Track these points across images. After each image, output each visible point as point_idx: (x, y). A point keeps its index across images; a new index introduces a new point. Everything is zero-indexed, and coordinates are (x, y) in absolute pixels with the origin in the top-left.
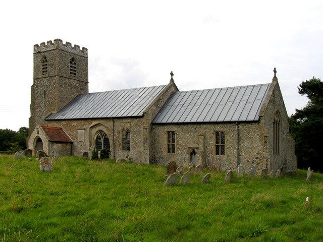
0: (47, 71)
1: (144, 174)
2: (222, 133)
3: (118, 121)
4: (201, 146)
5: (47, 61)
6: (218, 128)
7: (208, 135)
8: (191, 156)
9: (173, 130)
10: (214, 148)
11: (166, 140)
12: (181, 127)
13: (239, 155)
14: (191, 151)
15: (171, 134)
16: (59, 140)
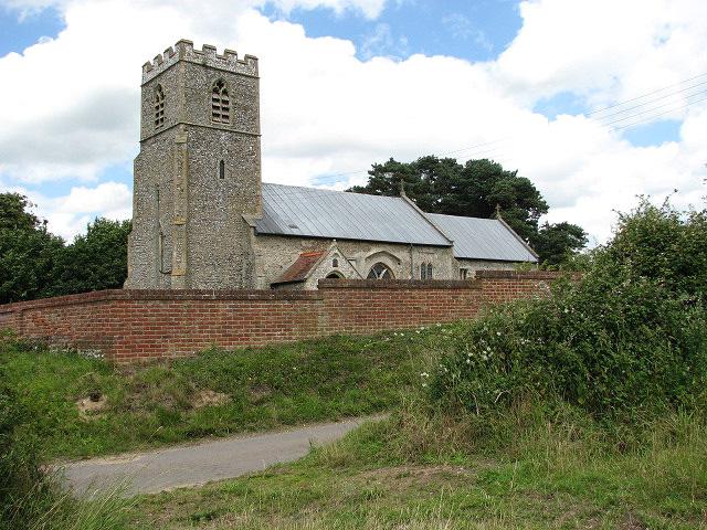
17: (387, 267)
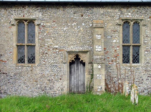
1: (49, 80)
4: (98, 48)
7: (110, 27)
8: (70, 68)
10: (120, 51)
11: (15, 38)
12: (52, 12)
14: (72, 57)
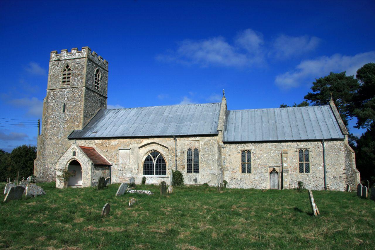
0: (69, 81)
2: (307, 150)
3: (182, 139)
5: (70, 70)
6: (302, 145)
8: (270, 176)
9: (249, 149)
13: (325, 172)
15: (246, 156)
16: (283, 144)
17: (160, 153)
